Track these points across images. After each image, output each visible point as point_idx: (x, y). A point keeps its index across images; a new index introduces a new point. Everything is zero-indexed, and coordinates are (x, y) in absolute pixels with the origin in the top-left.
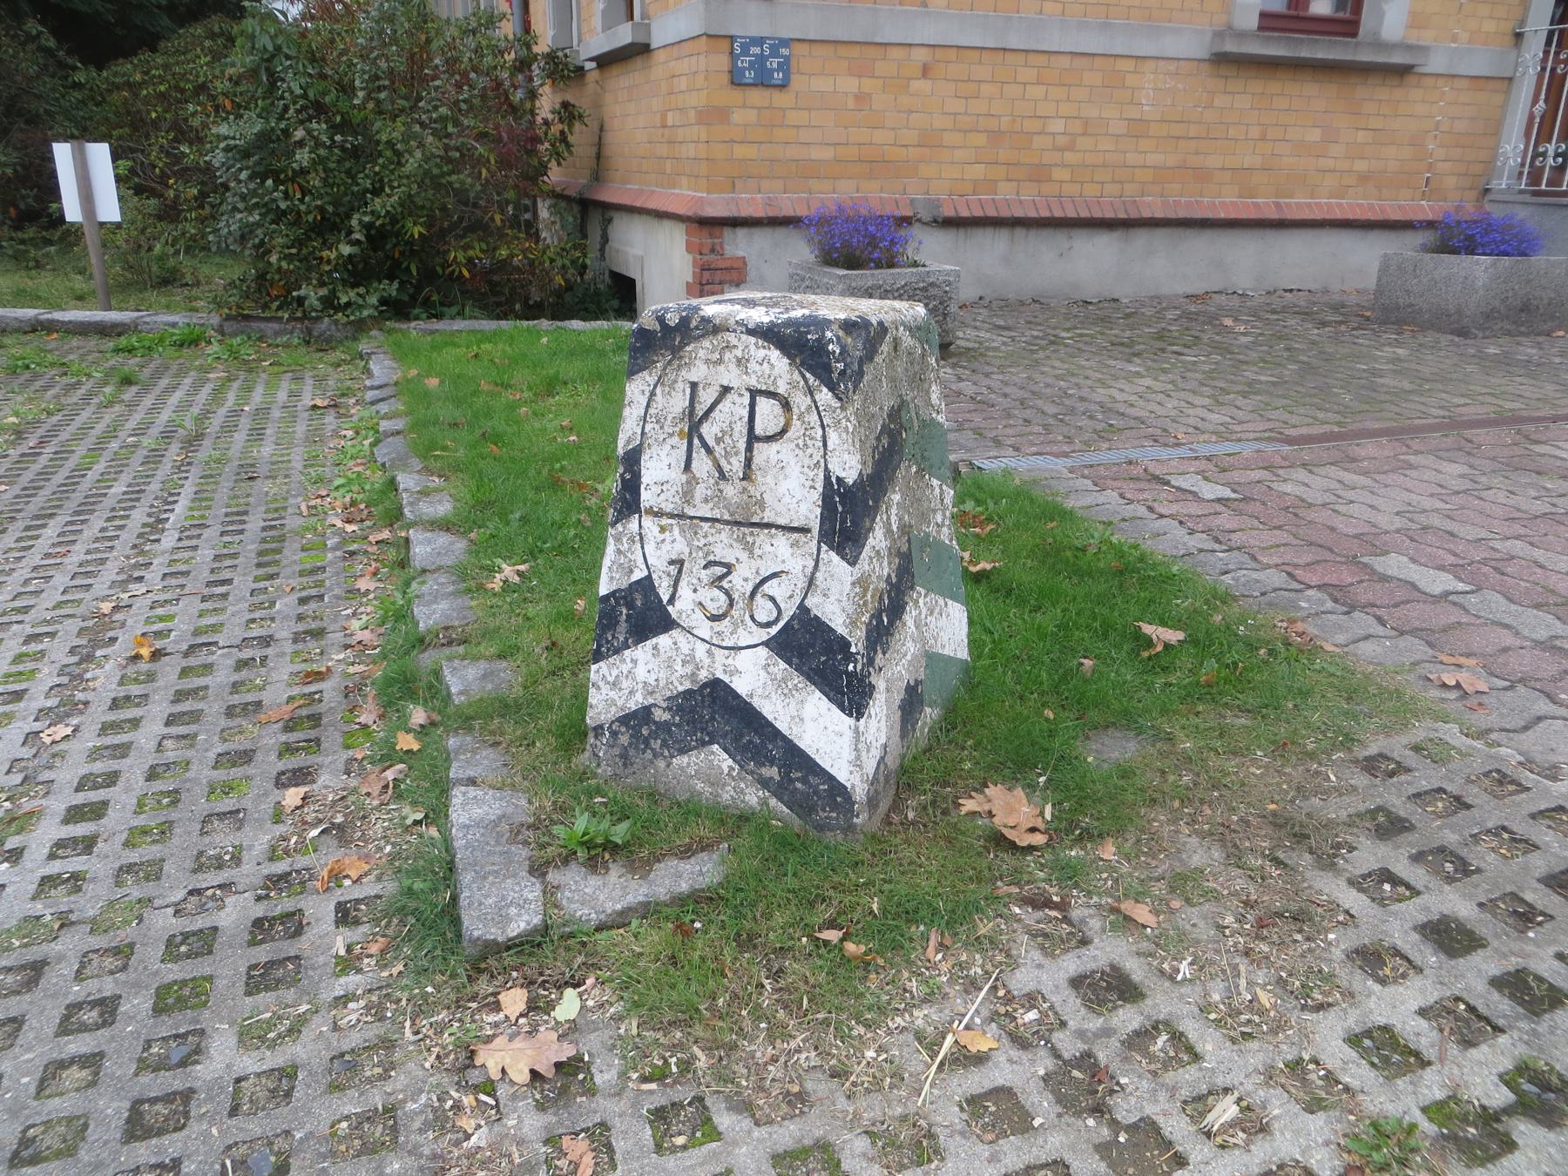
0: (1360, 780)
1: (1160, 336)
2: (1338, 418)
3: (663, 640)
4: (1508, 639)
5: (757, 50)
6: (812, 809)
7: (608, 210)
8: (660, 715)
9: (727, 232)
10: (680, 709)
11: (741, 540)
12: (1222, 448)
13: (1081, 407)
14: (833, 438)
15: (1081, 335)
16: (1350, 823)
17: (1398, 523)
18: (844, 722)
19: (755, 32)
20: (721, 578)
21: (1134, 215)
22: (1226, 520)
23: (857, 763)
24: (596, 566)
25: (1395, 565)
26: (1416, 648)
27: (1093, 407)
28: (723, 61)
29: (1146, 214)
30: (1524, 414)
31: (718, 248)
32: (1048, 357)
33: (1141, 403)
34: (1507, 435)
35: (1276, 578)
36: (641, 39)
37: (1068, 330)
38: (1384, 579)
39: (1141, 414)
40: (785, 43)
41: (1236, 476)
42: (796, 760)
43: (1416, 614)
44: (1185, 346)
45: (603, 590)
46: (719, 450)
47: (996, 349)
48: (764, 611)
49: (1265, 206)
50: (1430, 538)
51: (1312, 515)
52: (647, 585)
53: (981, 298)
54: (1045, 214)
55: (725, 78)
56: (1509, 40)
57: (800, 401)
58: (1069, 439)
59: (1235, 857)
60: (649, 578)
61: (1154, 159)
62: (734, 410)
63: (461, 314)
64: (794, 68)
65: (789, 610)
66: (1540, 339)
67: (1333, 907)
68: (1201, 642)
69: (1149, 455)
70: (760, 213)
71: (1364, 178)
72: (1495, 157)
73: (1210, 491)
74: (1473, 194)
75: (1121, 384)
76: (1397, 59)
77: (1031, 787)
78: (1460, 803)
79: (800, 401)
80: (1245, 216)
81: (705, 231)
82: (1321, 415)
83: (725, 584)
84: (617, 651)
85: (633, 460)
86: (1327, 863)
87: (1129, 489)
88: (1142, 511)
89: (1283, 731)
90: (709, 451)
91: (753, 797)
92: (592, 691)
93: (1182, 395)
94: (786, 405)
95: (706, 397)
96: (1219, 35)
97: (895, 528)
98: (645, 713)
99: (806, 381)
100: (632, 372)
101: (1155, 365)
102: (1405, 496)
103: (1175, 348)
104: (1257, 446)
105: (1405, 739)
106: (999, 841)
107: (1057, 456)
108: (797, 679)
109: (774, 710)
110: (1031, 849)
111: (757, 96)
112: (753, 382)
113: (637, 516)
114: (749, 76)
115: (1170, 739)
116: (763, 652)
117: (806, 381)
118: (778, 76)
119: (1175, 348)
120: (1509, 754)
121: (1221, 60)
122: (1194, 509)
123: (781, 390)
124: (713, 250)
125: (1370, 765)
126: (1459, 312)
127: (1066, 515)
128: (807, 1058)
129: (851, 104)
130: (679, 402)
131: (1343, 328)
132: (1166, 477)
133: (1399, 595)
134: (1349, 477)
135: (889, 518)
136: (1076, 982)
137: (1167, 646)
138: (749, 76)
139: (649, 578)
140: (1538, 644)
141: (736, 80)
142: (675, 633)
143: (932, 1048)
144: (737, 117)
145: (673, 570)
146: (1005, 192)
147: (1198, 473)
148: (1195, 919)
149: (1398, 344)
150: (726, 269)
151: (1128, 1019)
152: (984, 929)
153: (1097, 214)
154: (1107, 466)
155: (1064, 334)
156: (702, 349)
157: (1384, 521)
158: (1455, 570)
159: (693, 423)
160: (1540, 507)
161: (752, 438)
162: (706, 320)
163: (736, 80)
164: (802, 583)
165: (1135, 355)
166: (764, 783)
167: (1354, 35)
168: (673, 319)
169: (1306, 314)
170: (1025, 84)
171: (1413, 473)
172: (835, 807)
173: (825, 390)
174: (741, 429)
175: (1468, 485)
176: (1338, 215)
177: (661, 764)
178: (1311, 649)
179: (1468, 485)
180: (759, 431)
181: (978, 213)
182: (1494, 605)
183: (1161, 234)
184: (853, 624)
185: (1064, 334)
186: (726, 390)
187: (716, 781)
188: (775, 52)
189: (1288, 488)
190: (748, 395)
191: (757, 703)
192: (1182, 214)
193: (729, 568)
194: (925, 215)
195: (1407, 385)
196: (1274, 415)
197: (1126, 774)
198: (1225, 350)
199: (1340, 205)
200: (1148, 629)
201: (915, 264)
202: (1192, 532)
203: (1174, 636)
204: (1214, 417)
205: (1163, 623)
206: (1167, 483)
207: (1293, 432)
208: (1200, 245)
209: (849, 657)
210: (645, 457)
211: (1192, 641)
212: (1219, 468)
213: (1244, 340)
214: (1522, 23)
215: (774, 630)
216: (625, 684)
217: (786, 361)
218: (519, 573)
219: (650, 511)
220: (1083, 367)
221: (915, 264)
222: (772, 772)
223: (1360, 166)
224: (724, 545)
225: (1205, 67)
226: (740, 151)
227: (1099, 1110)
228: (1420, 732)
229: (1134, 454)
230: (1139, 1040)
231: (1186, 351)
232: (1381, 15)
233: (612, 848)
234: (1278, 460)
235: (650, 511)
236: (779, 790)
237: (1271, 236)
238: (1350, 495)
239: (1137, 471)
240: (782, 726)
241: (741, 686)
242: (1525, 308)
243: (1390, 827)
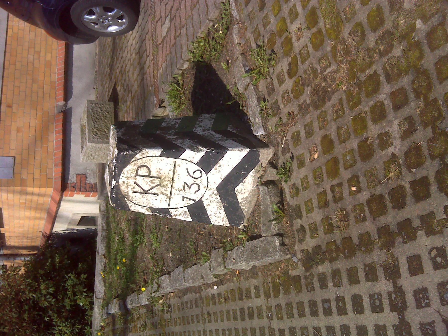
3: (205, 203)
20: (188, 186)
24: (182, 221)
31: (73, 185)
41: (163, 15)
48: (198, 174)
52: (189, 207)
53: (94, 88)
57: (140, 163)
62: (140, 180)
65: (198, 168)
70: (60, 168)
83: (190, 185)
90: (152, 188)
94: (140, 167)
95: (137, 189)
97: (176, 137)
99: (134, 161)
113: (170, 209)
117: (134, 161)
123: (136, 168)
129: (21, 134)
132: (163, 37)
135: (173, 139)
142: (203, 199)
145: (185, 199)
147: (162, 27)
150: (81, 182)
161: (149, 176)
170: (15, 69)
173: (137, 156)
180: (147, 174)
190: (137, 177)
193: (185, 183)
206: (165, 37)
210: (153, 207)
215: (203, 172)
217: (128, 166)
241: (219, 182)
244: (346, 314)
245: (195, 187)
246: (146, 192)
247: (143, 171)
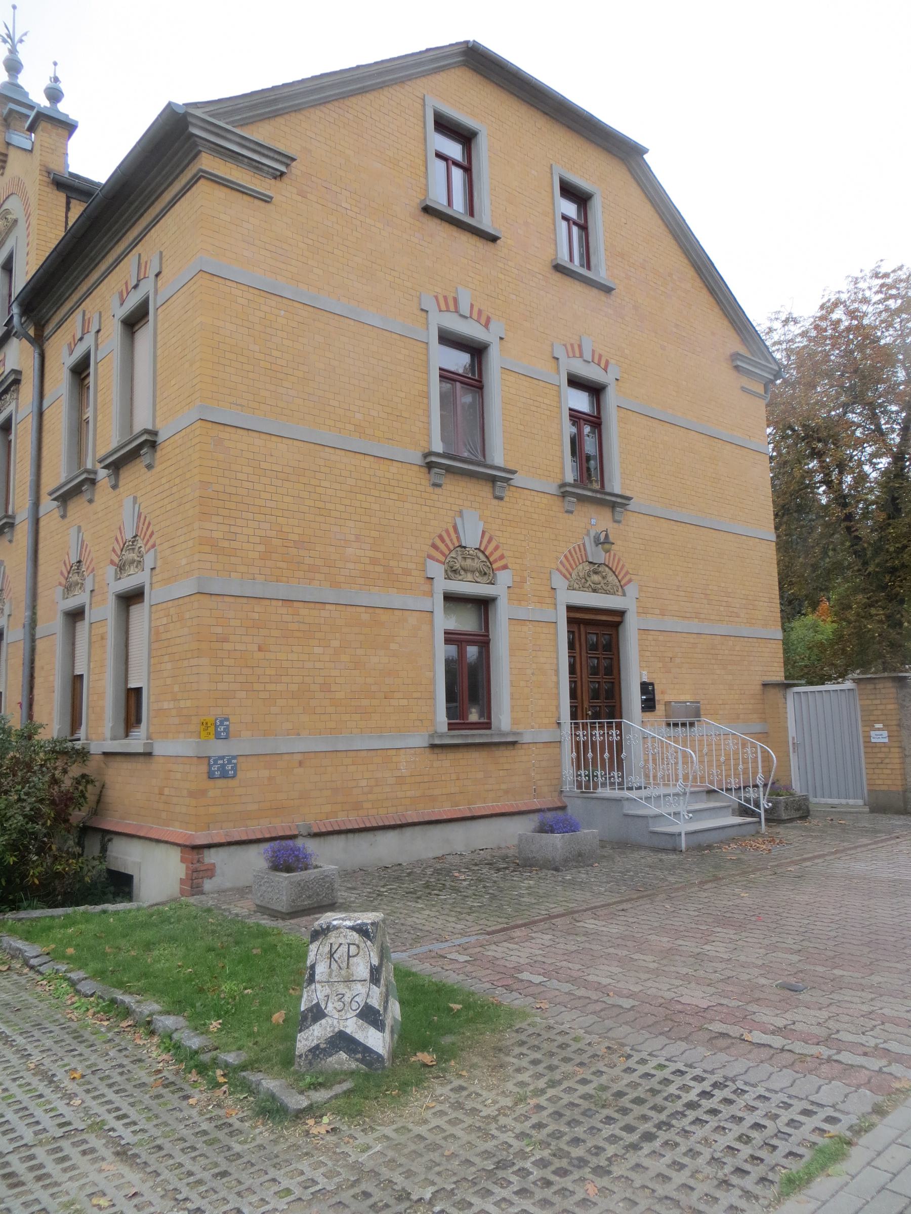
0: (514, 1035)
1: (427, 886)
2: (507, 920)
3: (323, 1021)
4: (557, 993)
5: (220, 762)
6: (372, 1065)
7: (107, 835)
8: (322, 1046)
9: (206, 852)
10: (329, 1042)
11: (347, 986)
12: (464, 940)
13: (404, 928)
14: (372, 954)
15: (391, 889)
16: (512, 1045)
17: (528, 961)
18: (379, 1034)
19: (220, 754)
21: (404, 822)
22: (469, 968)
23: (384, 1047)
25: (525, 976)
26: (530, 999)
27: (409, 928)
28: (204, 768)
29: (410, 821)
30: (576, 909)
32: (379, 904)
33: (427, 923)
34: (567, 920)
35: (488, 985)
36: (148, 751)
37: (383, 886)
38: (522, 981)
39: (429, 929)
40: (234, 757)
41: (470, 951)
42: (367, 1050)
43: (531, 990)
44: (440, 890)
45: (302, 1009)
46: (339, 961)
47: (354, 902)
49: (463, 810)
50: (537, 965)
51: (498, 962)
54: (362, 826)
55: (205, 776)
56: (555, 725)
57: (362, 945)
58: (404, 944)
59: (485, 1058)
60: (318, 1003)
61: (409, 794)
62: (344, 949)
63: (31, 907)
64: (238, 769)
65: (362, 1004)
66: (589, 868)
67: (509, 1063)
68: (467, 1007)
69: (437, 947)
70: (223, 840)
71: (506, 792)
72: (562, 776)
73: (462, 958)
74: (556, 794)
75: (417, 915)
76: (510, 739)
77: (428, 1052)
78: (539, 1035)
79: (362, 945)
80: (455, 816)
81: (195, 851)
82: (500, 920)
84: (308, 1028)
85: (313, 967)
86: (508, 1055)
87: (432, 961)
88: (439, 969)
89: (493, 1027)
91: (354, 1065)
92: (298, 1043)
93: (443, 917)
94: (358, 947)
96: (431, 736)
98: (317, 1047)
100: (312, 942)
101: (429, 903)
102: (530, 950)
103: (435, 892)
104: (476, 937)
105: (526, 1023)
106: (425, 1065)
107: (402, 952)
108: (366, 1025)
109: (359, 1036)
110: (432, 1066)
111: (221, 783)
112: (349, 941)
114: (217, 774)
115: (463, 1033)
116: (355, 1018)
118: (231, 773)
119: (435, 892)
120: (552, 1021)
121: (433, 746)
122: (457, 966)
124: (198, 861)
125: (517, 1031)
126: (554, 859)
127: (414, 974)
128: (392, 1115)
130: (327, 949)
131: (507, 871)
133: (526, 985)
134: (511, 946)
136: (451, 1090)
137: (458, 1010)
138: (217, 774)
139: (318, 1003)
140: (566, 993)
141: (211, 776)
143: (421, 1107)
144: (211, 793)
146: (341, 817)
148: (477, 1072)
149: (531, 878)
151: (465, 1093)
152: (426, 1085)
153: (387, 823)
154: (422, 954)
155: (382, 889)
156: (333, 934)
157: (522, 961)
158: (544, 975)
159: (331, 955)
160: (574, 948)
161: (349, 957)
162: (334, 926)
163: (211, 776)
164: (365, 996)
165: (419, 898)
166: (357, 1060)
167: (490, 728)
168: (324, 926)
169: (490, 864)
171: (533, 941)
172: (379, 1062)
174: (345, 954)
175: (552, 943)
176: (498, 811)
177: (323, 1062)
178: (499, 1005)
179: (552, 943)
181: (330, 829)
182: (555, 983)
183: (417, 829)
184: (380, 1006)
185: (382, 889)
186: (341, 944)
187: (341, 1063)
188: (229, 762)
189: (489, 953)
191: (353, 1035)
192: (427, 819)
193: (343, 995)
194: (304, 833)
195: (534, 901)
196: (481, 922)
197: (453, 1044)
198: (456, 890)
199: (497, 806)
200: (451, 1005)
201: (316, 867)
202: (458, 974)
203: (459, 1007)
204: (459, 926)
205: (455, 1003)
207: (489, 929)
208: (436, 831)
209: (380, 1015)
211: (465, 1007)
212: (464, 948)
213: (465, 883)
214: (559, 718)
216: (310, 1038)
218: (220, 1024)
219: (319, 982)
220: (397, 908)
221: (316, 867)
222: (359, 1056)
223: (504, 787)
224: (342, 988)
225: (427, 750)
226: (212, 810)
227: (462, 1109)
228: (529, 1020)
229: (431, 947)
230: (469, 1095)
231: (441, 893)
232: (500, 720)
233: (320, 1084)
234: (485, 942)
235: (319, 982)
236: (362, 1061)
237: (468, 824)
238: (511, 953)
239: (433, 954)
240: (361, 1040)
241: (348, 1031)
242: (580, 855)
243: (522, 1043)
244: (621, 613)
245: (339, 1005)
246: (332, 955)
247: (353, 949)
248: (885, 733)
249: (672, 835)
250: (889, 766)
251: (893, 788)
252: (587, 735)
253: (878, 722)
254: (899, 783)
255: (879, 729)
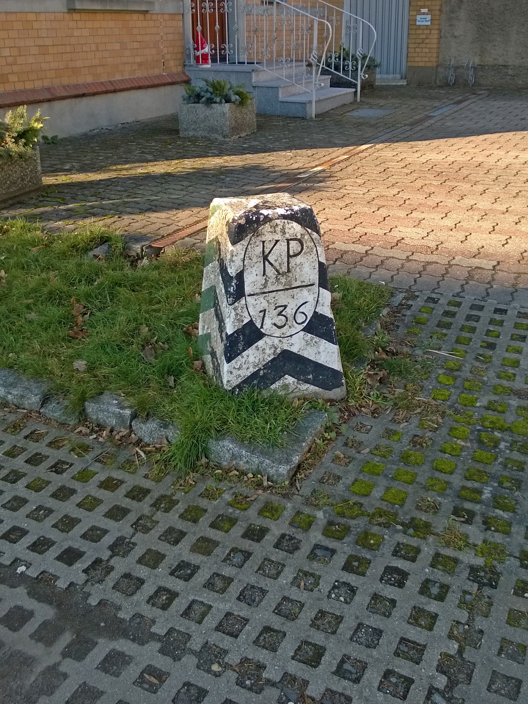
3: (260, 343)
42: (318, 367)
60: (251, 320)
62: (282, 247)
65: (310, 315)
71: (140, 64)
108: (317, 339)
109: (309, 354)
116: (302, 333)
139: (251, 320)
146: (139, 74)
161: (289, 256)
174: (285, 254)
186: (277, 241)
193: (285, 307)
219: (250, 295)
223: (138, 59)
235: (250, 295)
246: (265, 258)
247: (294, 246)
248: (429, 17)
249: (304, 104)
250: (428, 46)
251: (429, 64)
252: (201, 8)
253: (424, 7)
254: (434, 60)
255: (424, 14)
